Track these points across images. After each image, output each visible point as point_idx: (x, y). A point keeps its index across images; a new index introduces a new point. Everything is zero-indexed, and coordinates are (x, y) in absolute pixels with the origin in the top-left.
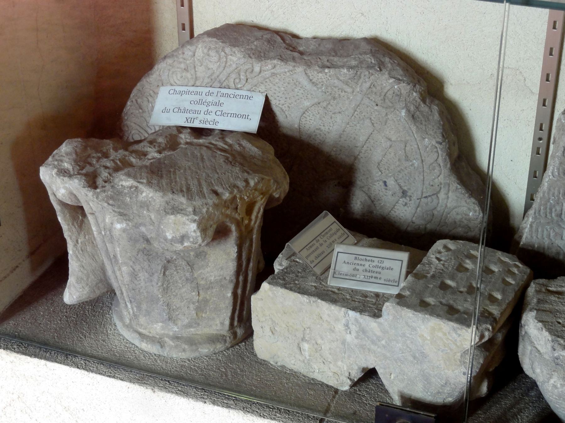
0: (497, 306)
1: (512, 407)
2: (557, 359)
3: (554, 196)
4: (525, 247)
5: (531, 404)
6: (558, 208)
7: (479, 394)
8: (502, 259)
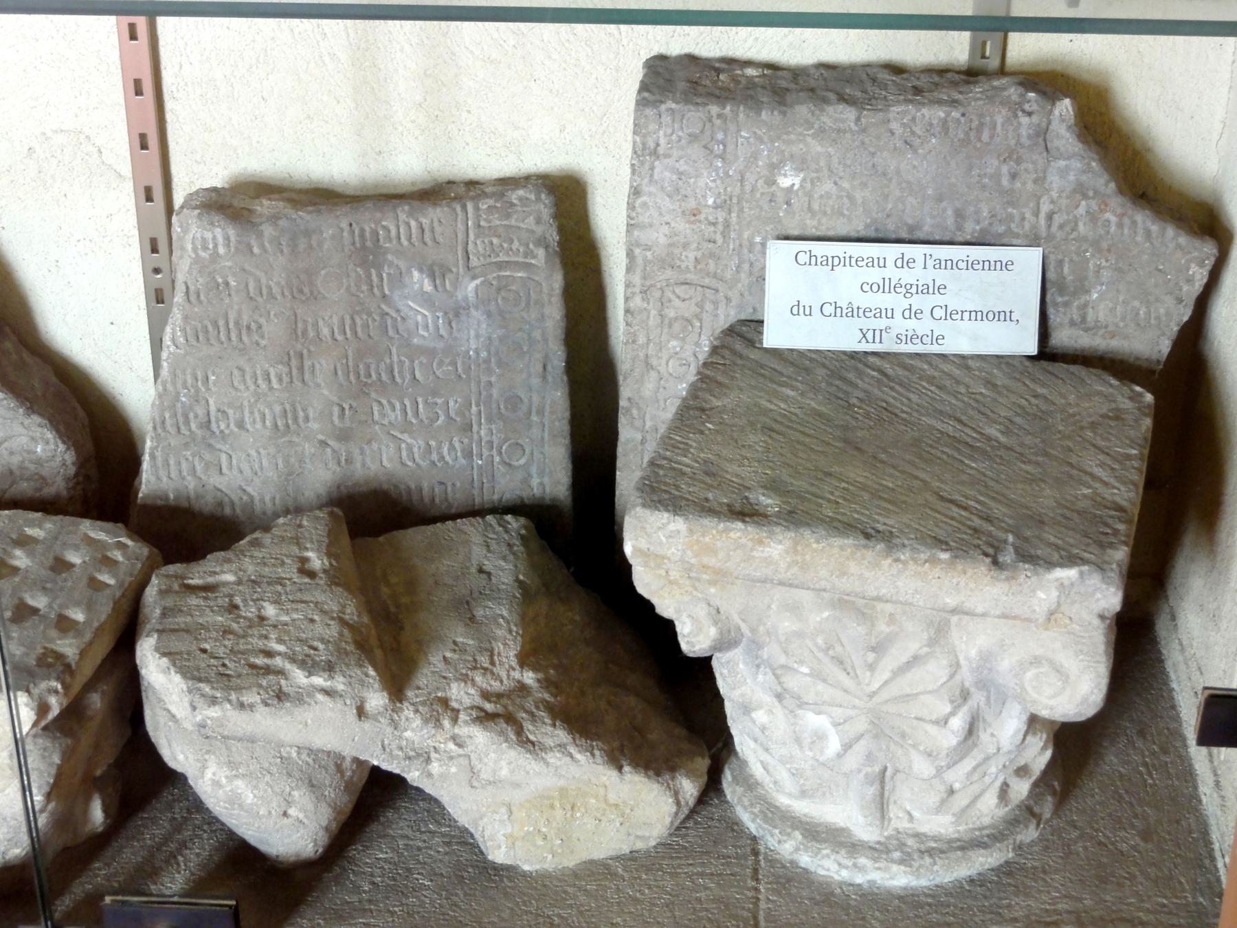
0: (75, 637)
1: (167, 839)
2: (204, 727)
3: (186, 388)
4: (149, 502)
5: (205, 827)
6: (201, 411)
7: (88, 828)
8: (92, 534)
